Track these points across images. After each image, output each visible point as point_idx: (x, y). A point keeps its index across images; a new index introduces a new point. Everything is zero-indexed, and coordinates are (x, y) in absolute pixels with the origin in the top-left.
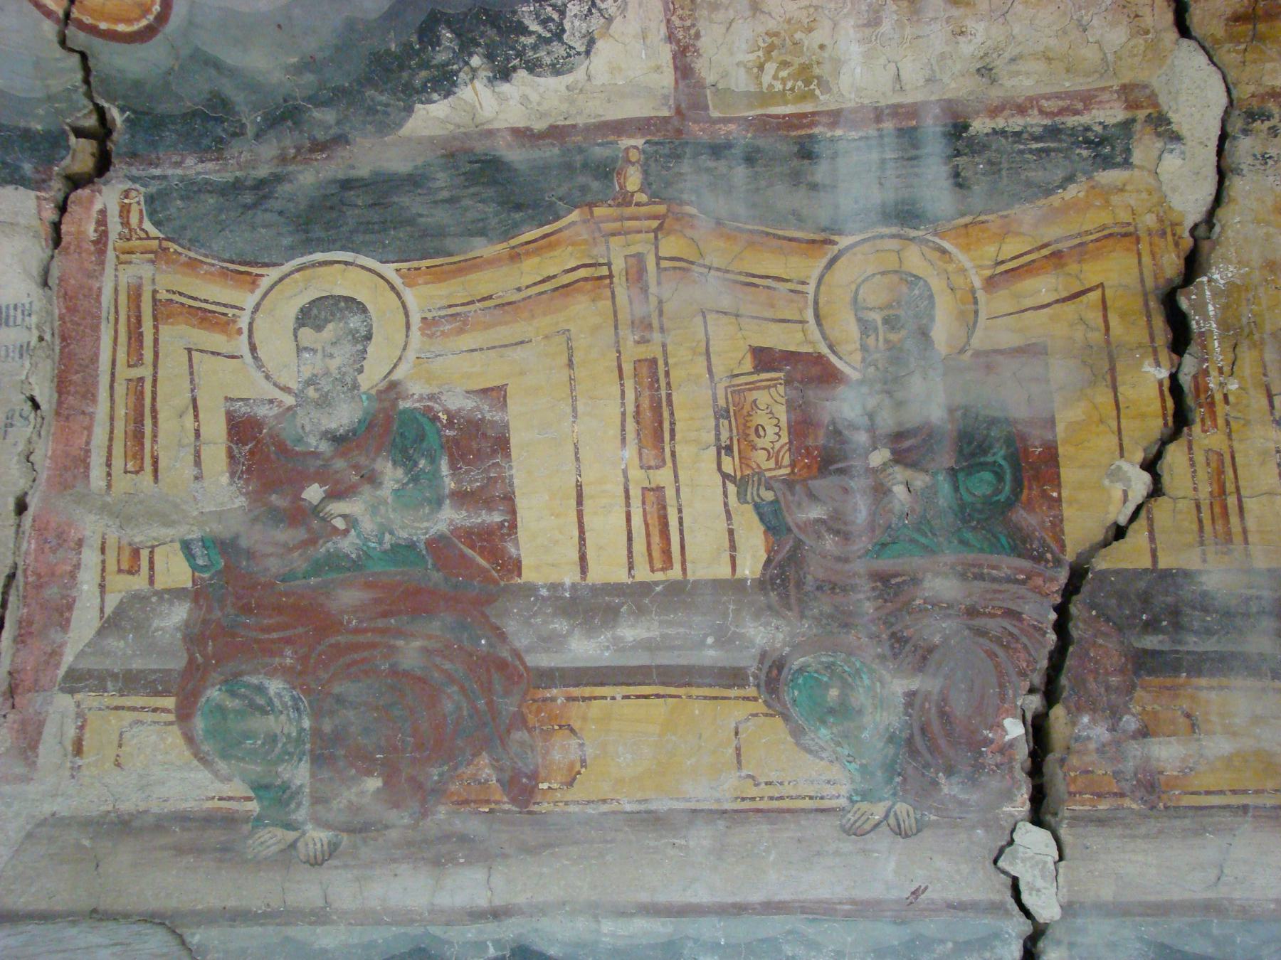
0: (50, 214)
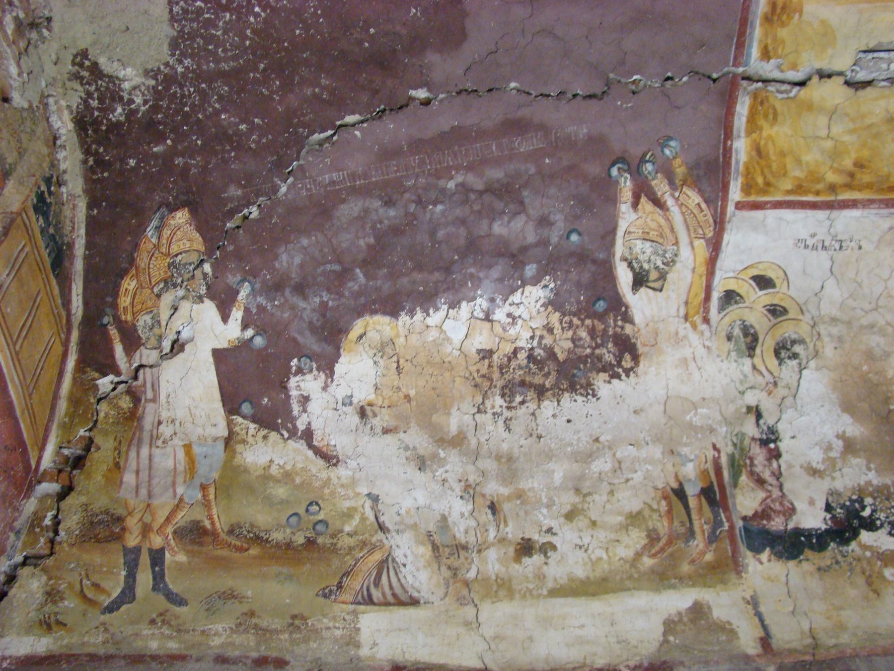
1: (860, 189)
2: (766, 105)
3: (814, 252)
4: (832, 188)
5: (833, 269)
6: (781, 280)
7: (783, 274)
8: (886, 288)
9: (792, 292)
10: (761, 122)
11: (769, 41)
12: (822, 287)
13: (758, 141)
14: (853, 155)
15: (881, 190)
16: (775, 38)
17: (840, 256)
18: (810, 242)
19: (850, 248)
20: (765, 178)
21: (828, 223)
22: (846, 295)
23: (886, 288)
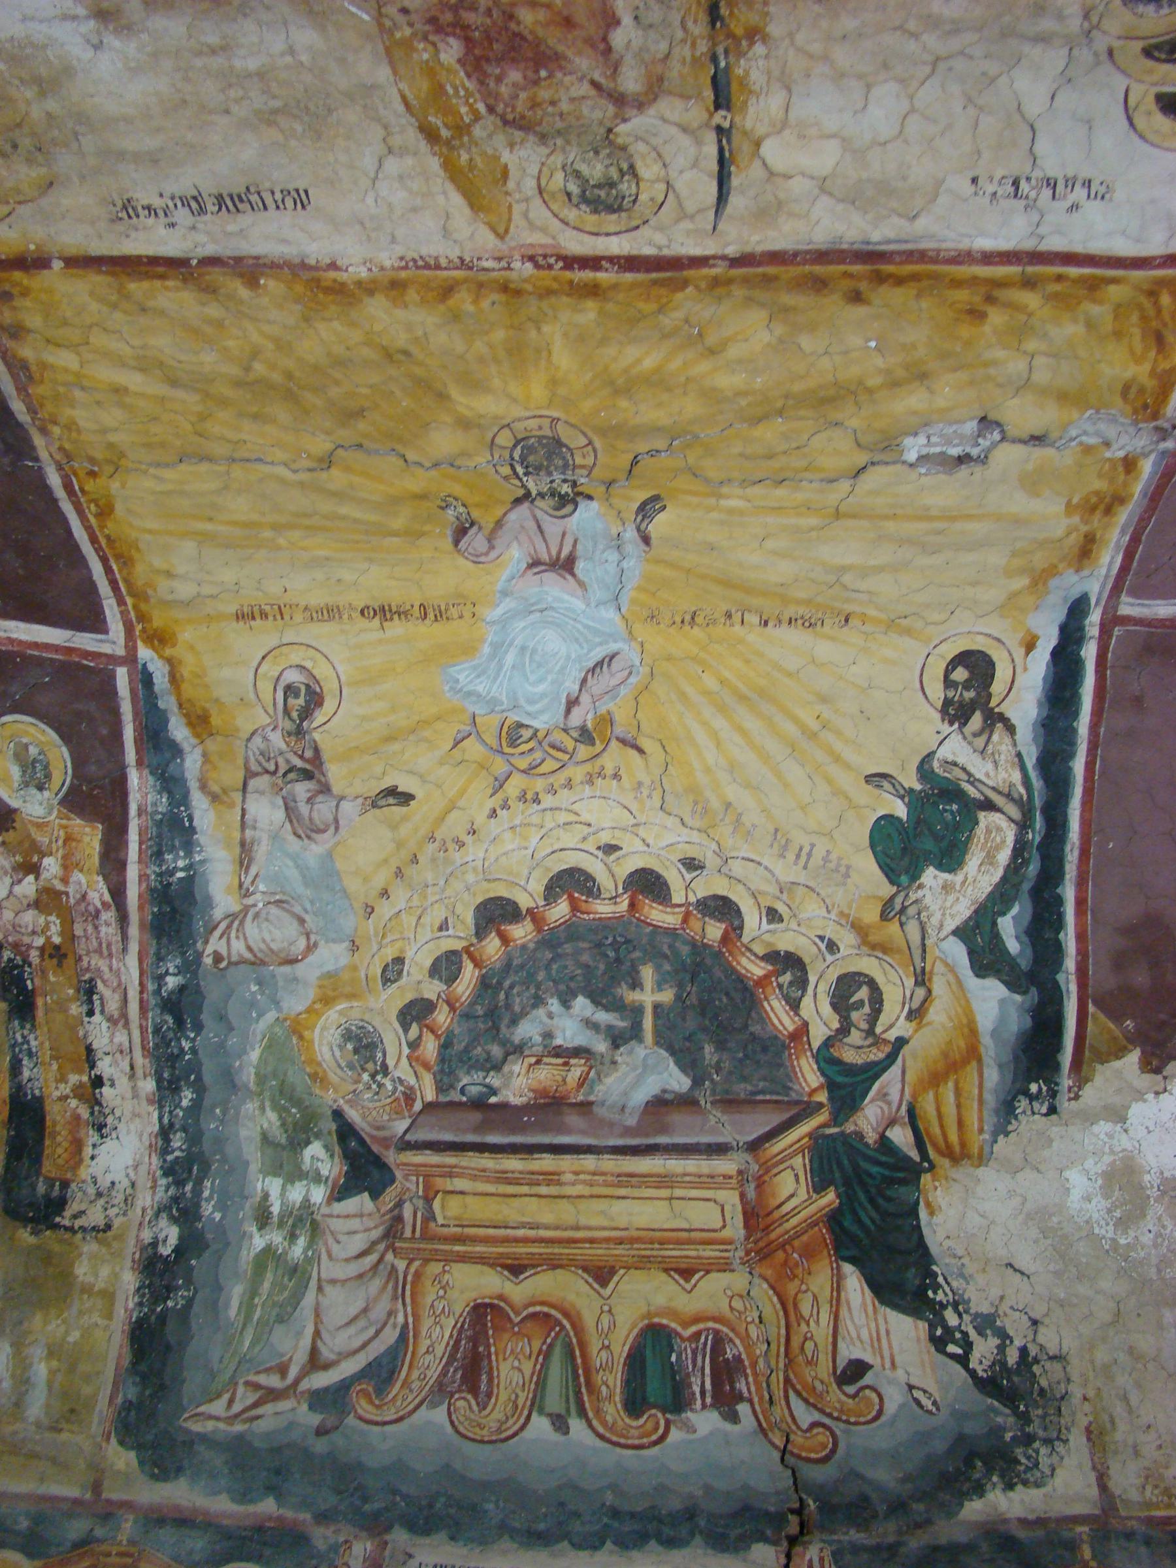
0: (783, 1560)
1: (974, 281)
2: (1138, 404)
3: (1070, 174)
4: (1029, 283)
5: (1030, 135)
6: (1142, 108)
7: (1136, 121)
8: (911, 98)
9: (1121, 82)
10: (1151, 384)
11: (1122, 477)
12: (1053, 98)
13: (1160, 357)
14: (987, 329)
15: (935, 277)
16: (1112, 481)
17: (1017, 165)
18: (1080, 193)
19: (996, 180)
20: (1155, 303)
21: (1042, 230)
22: (1003, 81)
23: (911, 98)
